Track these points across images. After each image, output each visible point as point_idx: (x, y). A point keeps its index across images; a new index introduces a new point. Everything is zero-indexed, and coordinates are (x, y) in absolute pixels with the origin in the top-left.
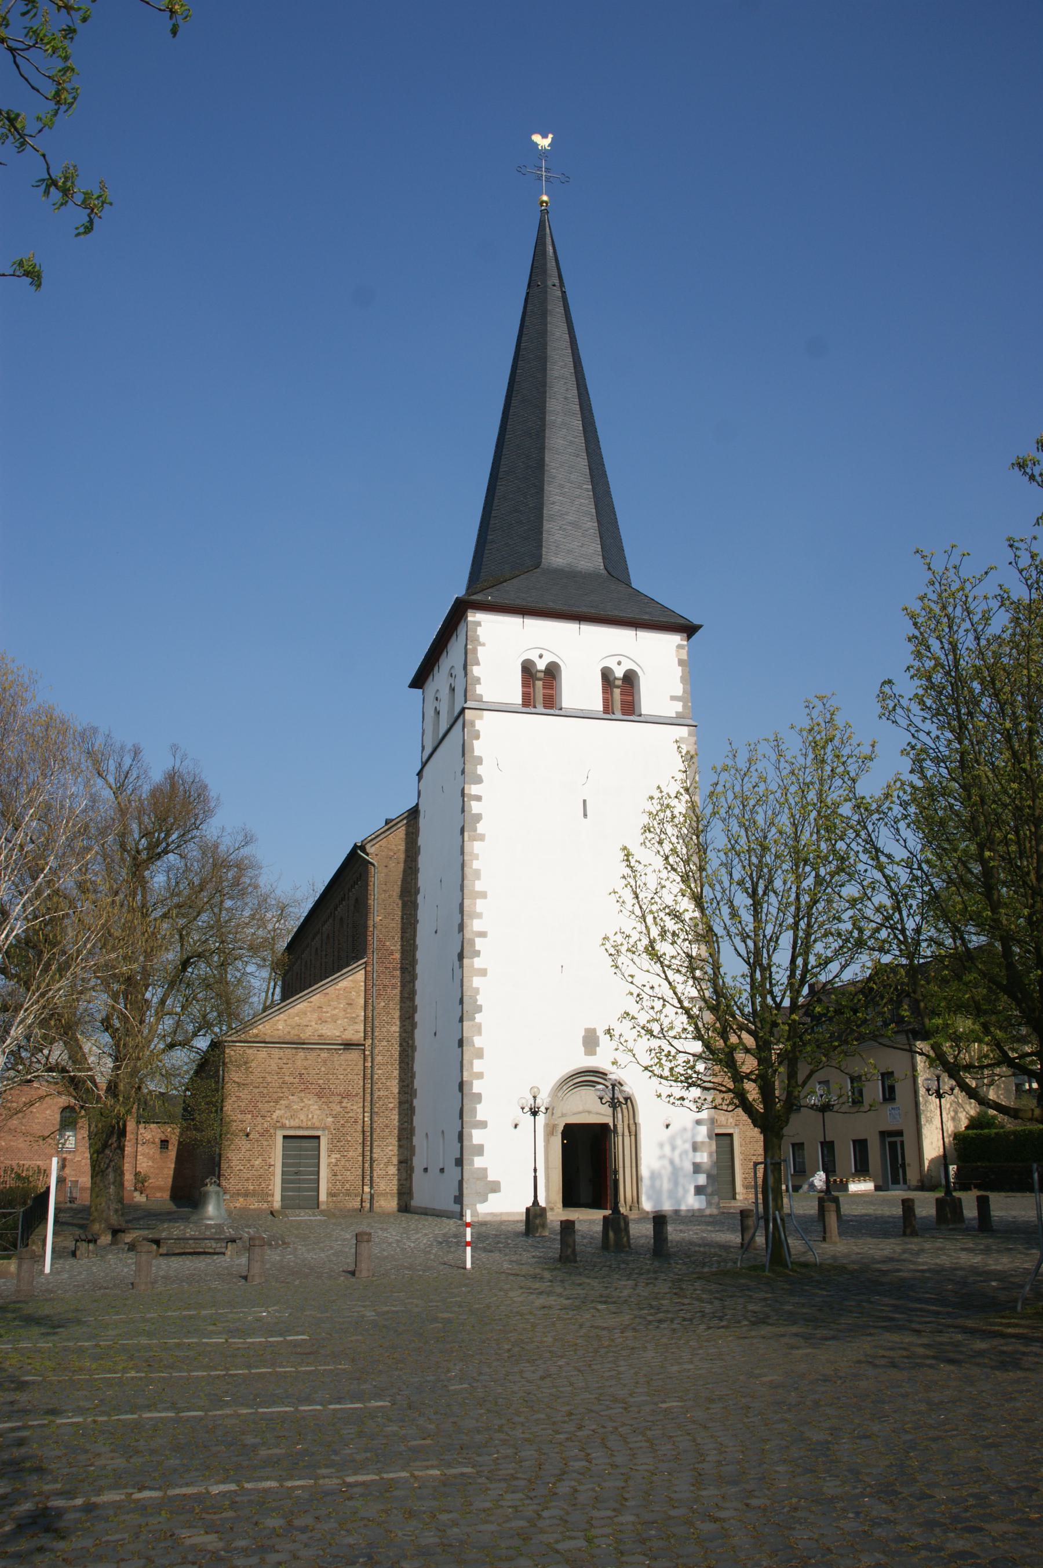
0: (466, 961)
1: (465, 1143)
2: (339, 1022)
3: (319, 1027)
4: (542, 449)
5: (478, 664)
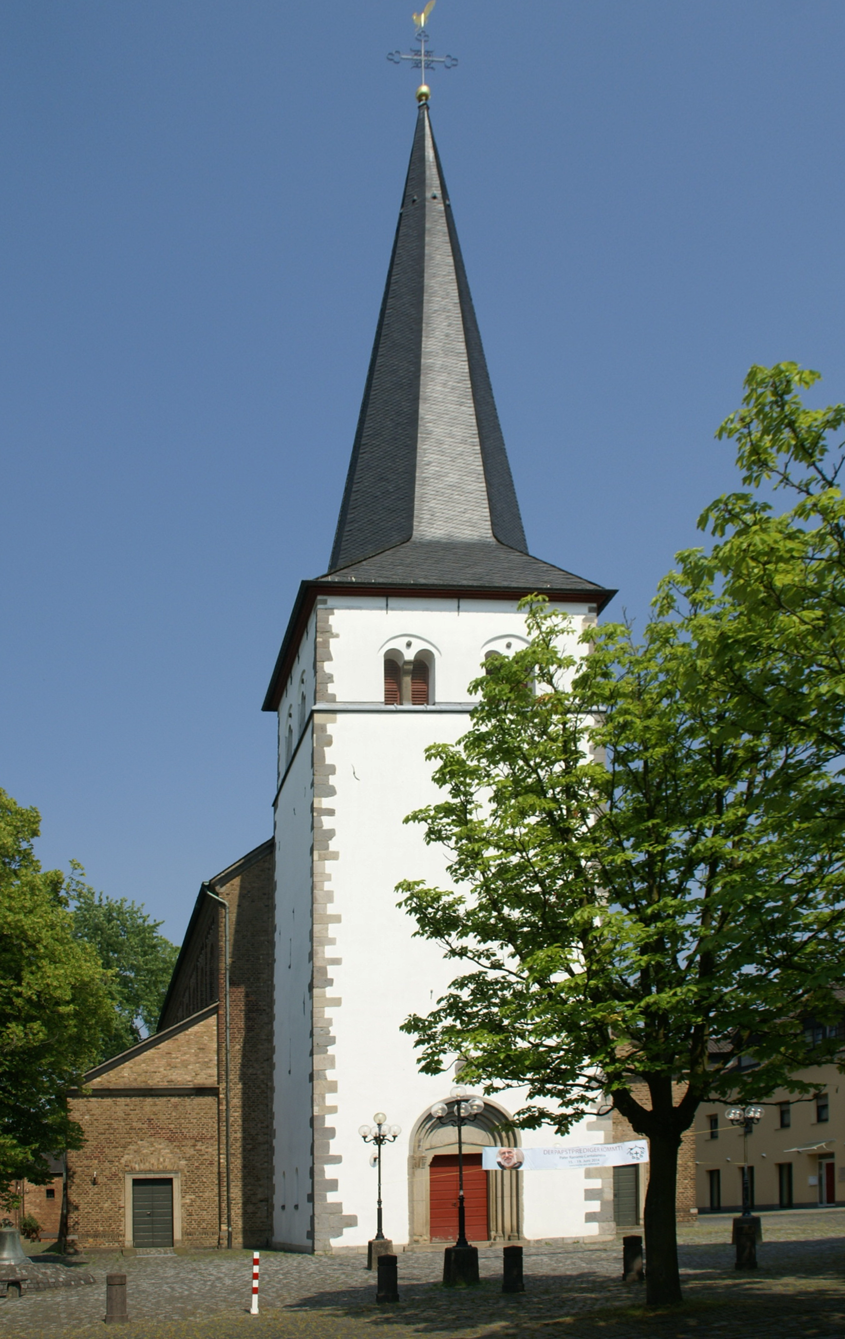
0: (316, 991)
1: (316, 1178)
2: (190, 1067)
3: (169, 1073)
4: (415, 400)
5: (330, 658)
